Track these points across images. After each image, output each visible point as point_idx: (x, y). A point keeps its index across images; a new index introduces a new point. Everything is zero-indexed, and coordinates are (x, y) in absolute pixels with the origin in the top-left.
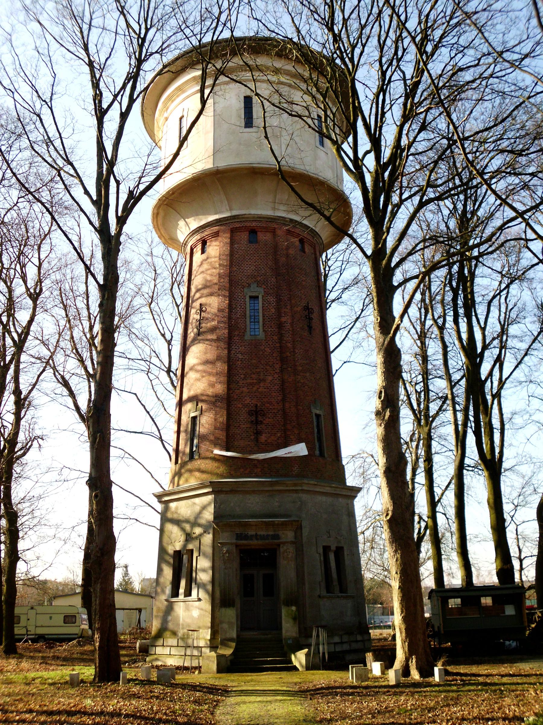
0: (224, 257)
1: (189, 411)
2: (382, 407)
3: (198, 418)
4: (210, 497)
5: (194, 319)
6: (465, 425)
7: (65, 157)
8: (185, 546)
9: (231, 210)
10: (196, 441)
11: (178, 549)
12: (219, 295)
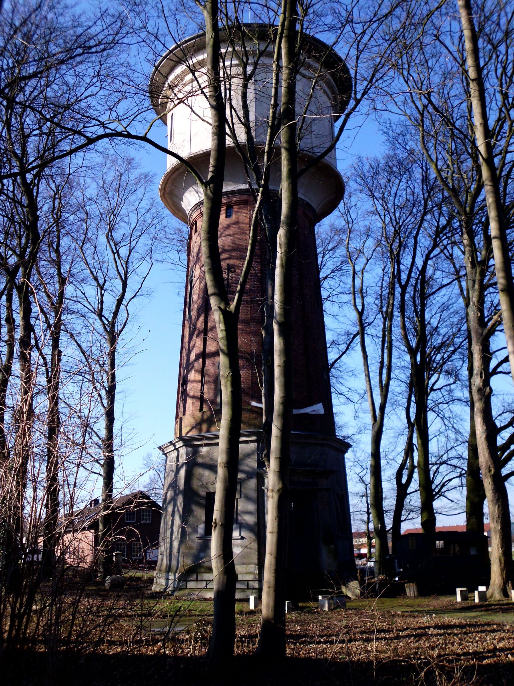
2: (483, 385)
4: (253, 446)
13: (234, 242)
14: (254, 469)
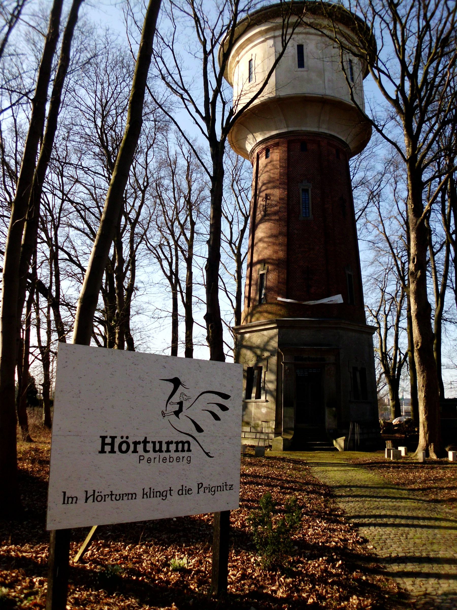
0: (283, 161)
1: (258, 270)
2: (415, 269)
3: (265, 276)
4: (276, 331)
5: (261, 204)
6: (445, 286)
7: (182, 86)
8: (256, 364)
9: (288, 127)
10: (263, 291)
11: (251, 366)
12: (280, 188)
13: (270, 177)
14: (275, 348)
